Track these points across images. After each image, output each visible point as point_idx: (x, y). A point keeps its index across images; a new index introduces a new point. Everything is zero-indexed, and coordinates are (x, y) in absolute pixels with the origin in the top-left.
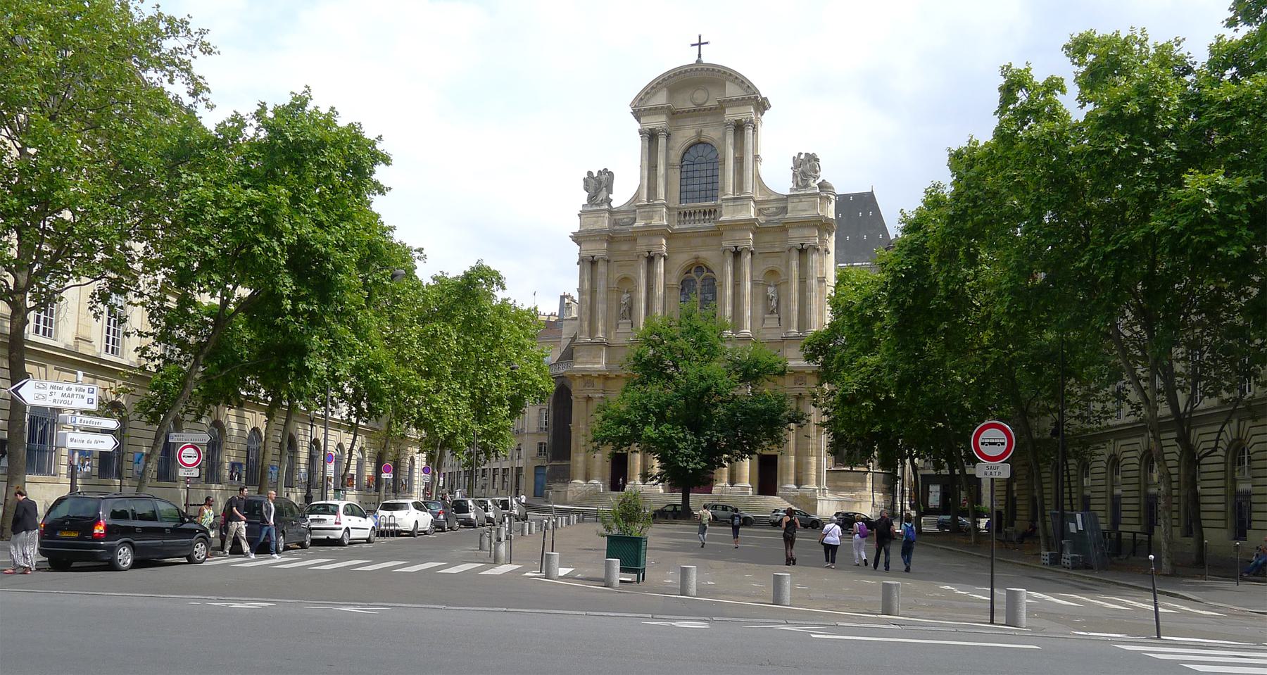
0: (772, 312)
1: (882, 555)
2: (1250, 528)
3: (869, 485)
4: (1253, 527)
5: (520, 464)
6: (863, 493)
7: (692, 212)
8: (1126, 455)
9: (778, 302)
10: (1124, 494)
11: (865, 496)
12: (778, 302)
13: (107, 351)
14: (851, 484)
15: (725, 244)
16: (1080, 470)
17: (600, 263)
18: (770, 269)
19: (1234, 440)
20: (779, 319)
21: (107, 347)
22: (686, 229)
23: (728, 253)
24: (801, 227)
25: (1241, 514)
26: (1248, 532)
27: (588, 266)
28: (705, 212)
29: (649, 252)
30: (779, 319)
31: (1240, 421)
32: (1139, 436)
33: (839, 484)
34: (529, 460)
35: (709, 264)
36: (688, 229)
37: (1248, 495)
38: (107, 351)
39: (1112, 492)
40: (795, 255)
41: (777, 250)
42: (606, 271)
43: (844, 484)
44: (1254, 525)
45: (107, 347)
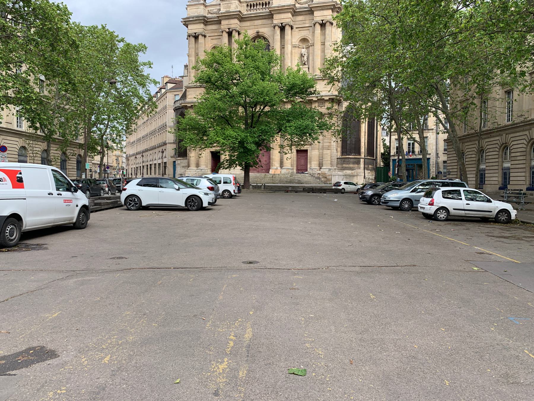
0: (305, 64)
1: (391, 208)
2: (509, 184)
3: (362, 165)
4: (510, 184)
5: (165, 160)
6: (359, 171)
7: (255, 4)
8: (488, 147)
9: (308, 58)
10: (488, 168)
11: (360, 173)
12: (308, 58)
13: (18, 127)
14: (351, 166)
15: (275, 22)
16: (529, 147)
17: (200, 37)
18: (303, 37)
19: (503, 144)
20: (309, 68)
21: (18, 125)
22: (251, 14)
23: (277, 28)
24: (322, 10)
25: (481, 178)
26: (508, 186)
27: (193, 39)
28: (266, 4)
29: (229, 29)
30: (309, 68)
31: (463, 143)
32: (526, 130)
33: (344, 165)
34: (170, 158)
35: (266, 36)
36: (253, 14)
37: (484, 170)
38: (18, 127)
39: (502, 165)
40: (318, 27)
41: (307, 25)
42: (204, 42)
43: (347, 166)
44: (486, 182)
45: (18, 125)
